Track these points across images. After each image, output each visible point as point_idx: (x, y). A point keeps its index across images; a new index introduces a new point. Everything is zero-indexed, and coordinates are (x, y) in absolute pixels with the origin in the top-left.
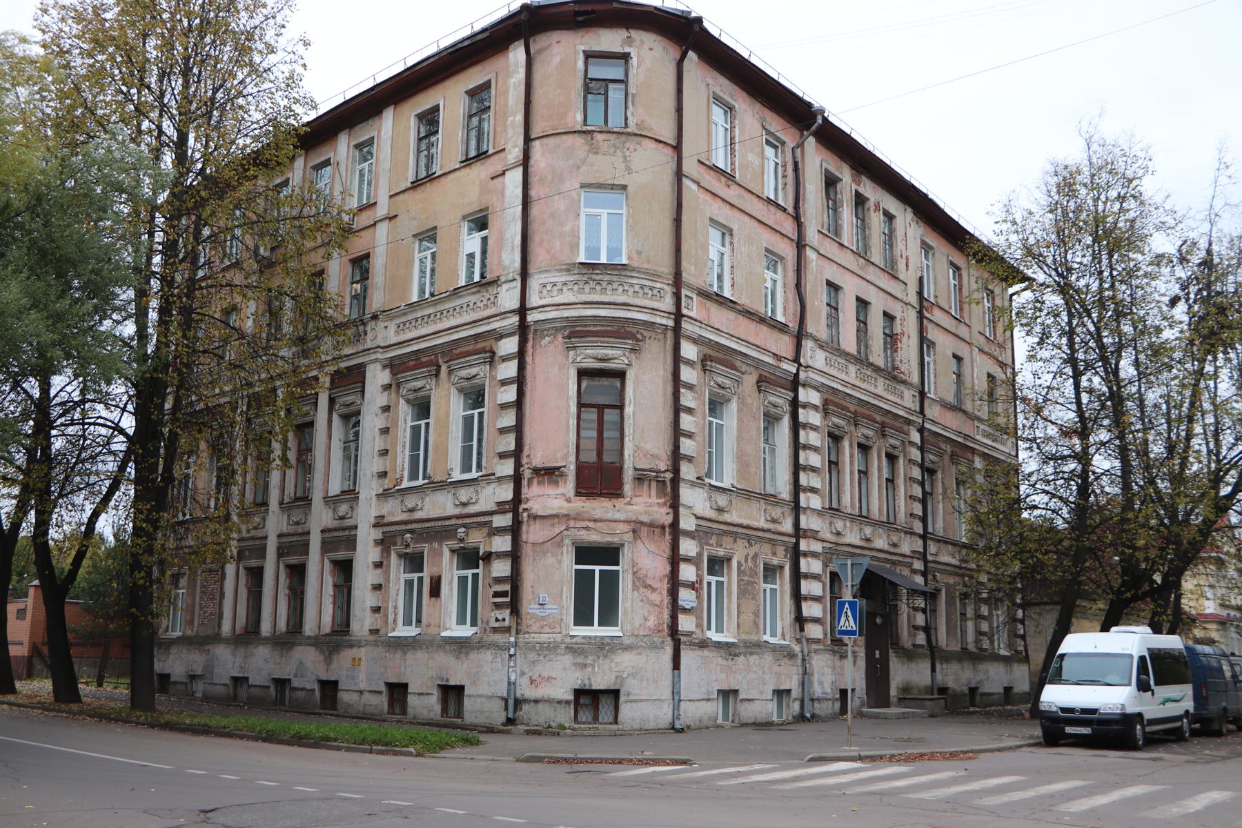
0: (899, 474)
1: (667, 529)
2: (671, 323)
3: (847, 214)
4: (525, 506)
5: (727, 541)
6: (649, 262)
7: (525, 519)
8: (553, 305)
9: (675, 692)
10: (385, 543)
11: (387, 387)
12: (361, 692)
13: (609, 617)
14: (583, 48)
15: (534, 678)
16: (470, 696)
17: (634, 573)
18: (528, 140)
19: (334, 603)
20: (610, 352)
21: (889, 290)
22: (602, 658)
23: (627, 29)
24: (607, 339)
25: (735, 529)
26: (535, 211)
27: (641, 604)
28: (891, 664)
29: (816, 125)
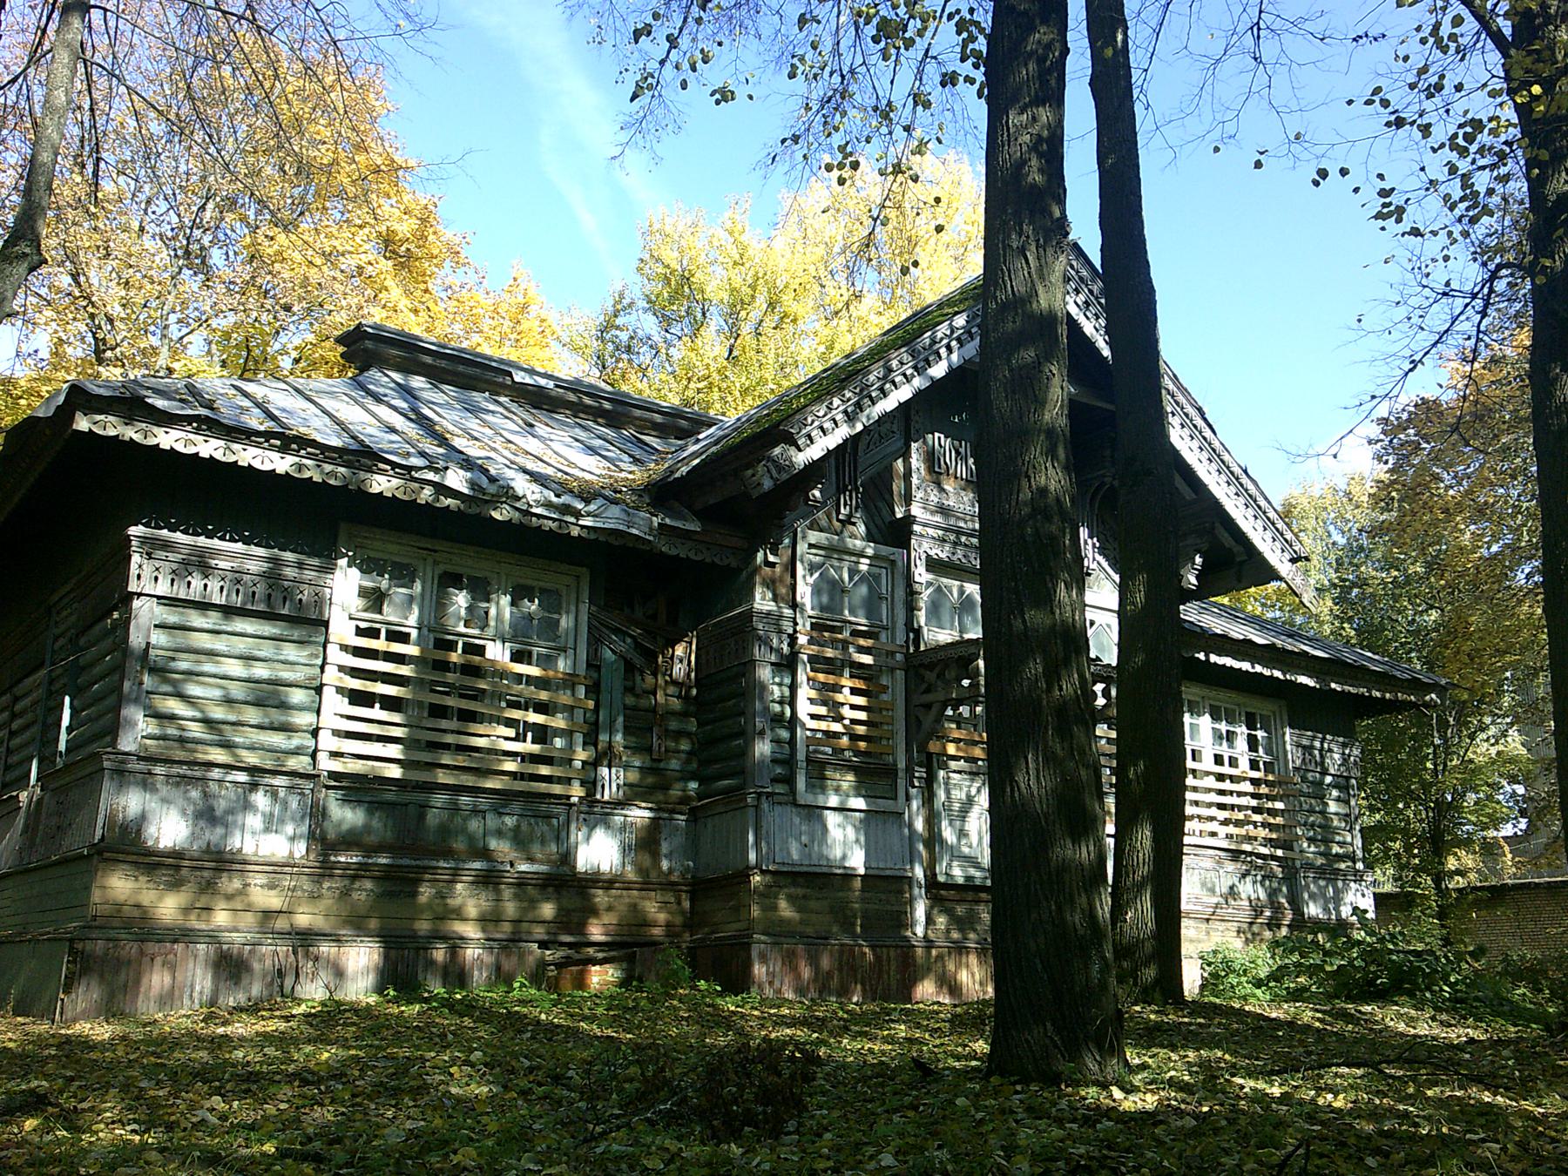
14: (342, 320)
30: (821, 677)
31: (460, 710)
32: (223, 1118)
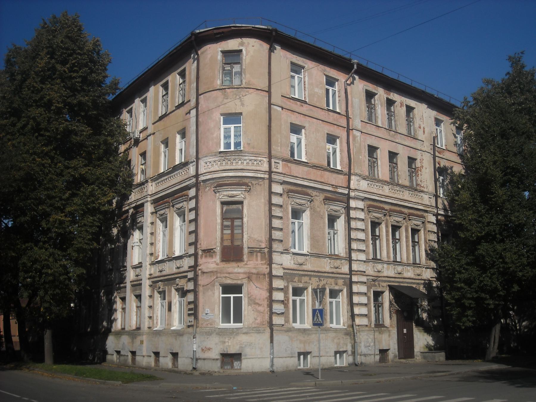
0: (421, 238)
1: (266, 276)
2: (267, 176)
3: (381, 111)
4: (200, 268)
5: (306, 279)
6: (253, 148)
7: (200, 274)
8: (209, 172)
9: (272, 353)
10: (153, 286)
11: (152, 213)
12: (144, 356)
13: (238, 318)
14: (220, 50)
15: (203, 348)
16: (180, 357)
17: (249, 298)
18: (198, 95)
19: (137, 315)
20: (235, 193)
21: (411, 146)
22: (232, 338)
23: (241, 38)
24: (233, 187)
25: (309, 273)
26: (200, 129)
27: (253, 312)
28: (415, 336)
29: (354, 69)
30: (18, 87)
31: (230, 143)
32: (486, 132)
